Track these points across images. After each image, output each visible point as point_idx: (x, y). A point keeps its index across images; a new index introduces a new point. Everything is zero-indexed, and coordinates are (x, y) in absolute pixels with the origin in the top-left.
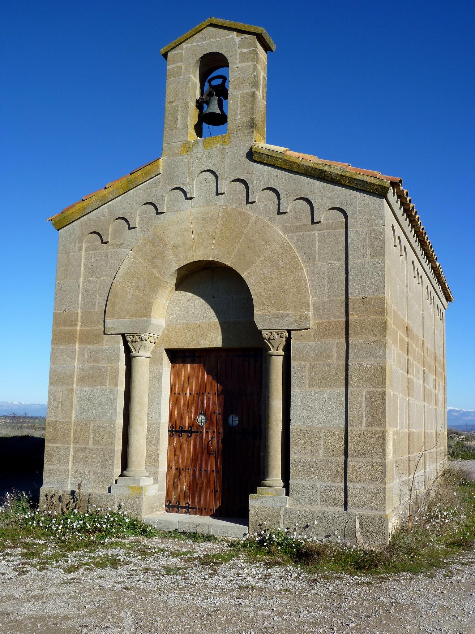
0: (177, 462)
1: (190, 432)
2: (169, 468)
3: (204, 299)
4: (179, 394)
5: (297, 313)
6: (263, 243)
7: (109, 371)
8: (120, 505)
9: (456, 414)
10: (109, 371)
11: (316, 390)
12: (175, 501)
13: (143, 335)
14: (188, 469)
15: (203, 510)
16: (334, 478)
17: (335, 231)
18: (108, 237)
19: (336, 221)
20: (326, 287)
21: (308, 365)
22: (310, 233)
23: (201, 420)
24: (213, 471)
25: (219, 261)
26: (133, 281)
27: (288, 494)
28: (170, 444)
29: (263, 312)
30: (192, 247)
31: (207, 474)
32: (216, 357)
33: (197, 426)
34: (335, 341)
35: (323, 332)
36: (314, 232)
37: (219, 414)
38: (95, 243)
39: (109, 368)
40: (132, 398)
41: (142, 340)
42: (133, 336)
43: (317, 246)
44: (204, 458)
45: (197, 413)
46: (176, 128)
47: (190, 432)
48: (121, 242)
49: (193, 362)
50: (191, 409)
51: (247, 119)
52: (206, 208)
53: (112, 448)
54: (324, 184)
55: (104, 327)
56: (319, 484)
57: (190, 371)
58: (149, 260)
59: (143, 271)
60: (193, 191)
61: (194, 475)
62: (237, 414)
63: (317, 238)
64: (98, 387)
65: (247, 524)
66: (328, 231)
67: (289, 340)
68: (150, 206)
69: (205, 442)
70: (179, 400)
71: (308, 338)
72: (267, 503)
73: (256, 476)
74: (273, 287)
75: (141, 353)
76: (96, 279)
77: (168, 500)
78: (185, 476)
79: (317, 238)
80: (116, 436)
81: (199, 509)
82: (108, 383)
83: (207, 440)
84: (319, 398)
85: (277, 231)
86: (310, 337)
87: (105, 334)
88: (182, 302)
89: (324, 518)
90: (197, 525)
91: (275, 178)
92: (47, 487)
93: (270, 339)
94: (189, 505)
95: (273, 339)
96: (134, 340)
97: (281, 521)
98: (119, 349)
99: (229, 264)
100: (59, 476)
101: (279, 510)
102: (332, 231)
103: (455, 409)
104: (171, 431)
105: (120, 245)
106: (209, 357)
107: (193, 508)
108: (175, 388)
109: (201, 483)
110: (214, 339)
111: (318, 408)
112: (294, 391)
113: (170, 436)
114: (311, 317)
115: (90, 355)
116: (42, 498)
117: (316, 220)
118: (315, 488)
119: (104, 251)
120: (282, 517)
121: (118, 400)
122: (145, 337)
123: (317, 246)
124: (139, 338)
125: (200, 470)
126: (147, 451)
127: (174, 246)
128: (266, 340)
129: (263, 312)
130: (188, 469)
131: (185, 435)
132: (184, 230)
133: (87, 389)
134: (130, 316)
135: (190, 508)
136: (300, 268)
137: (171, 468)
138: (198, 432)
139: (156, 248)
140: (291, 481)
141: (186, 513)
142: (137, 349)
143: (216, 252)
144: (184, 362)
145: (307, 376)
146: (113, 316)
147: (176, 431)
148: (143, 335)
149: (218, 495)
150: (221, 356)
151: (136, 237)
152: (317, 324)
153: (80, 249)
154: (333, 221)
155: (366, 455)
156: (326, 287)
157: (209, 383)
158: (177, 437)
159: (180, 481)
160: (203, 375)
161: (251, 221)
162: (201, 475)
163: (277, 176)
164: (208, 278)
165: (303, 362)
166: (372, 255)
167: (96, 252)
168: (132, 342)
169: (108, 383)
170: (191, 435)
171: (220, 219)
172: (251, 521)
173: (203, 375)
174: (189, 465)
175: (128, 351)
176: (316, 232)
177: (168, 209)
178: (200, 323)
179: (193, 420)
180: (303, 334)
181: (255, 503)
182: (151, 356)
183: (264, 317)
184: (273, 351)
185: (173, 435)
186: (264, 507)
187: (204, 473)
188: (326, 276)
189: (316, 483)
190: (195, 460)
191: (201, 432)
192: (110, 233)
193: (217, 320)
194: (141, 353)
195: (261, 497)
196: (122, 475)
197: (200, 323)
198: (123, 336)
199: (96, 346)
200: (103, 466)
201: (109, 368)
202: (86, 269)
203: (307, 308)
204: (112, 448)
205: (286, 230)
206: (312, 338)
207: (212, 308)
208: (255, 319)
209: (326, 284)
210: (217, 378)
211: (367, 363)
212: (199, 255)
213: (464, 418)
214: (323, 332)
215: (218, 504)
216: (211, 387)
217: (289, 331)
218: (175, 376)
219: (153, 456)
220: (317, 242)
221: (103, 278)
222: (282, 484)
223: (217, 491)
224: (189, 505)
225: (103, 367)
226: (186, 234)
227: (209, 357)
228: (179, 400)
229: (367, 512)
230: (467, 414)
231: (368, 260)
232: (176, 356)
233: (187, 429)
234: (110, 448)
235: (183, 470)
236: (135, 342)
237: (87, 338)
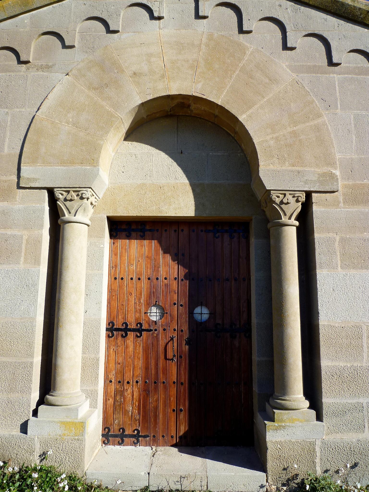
0: (121, 372)
1: (139, 330)
2: (108, 381)
3: (167, 153)
4: (122, 279)
5: (319, 170)
6: (267, 81)
7: (24, 242)
8: (44, 454)
10: (24, 242)
11: (353, 272)
12: (117, 428)
13: (84, 191)
14: (137, 382)
15: (161, 438)
17: (359, 77)
18: (29, 54)
19: (359, 65)
20: (354, 142)
21: (338, 238)
22: (327, 76)
23: (154, 314)
24: (174, 383)
25: (204, 97)
26: (70, 115)
27: (319, 418)
28: (108, 348)
29: (272, 167)
30: (163, 76)
31: (165, 387)
32: (175, 231)
33: (150, 322)
36: (332, 75)
37: (181, 305)
38: (6, 63)
39: (25, 237)
40: (63, 283)
41: (82, 198)
42: (68, 192)
43: (338, 92)
44: (161, 365)
45: (149, 305)
47: (139, 330)
48: (50, 64)
49: (143, 237)
50: (140, 299)
52: (183, 31)
53: (29, 360)
54: (342, 22)
55: (19, 177)
57: (139, 250)
58: (95, 89)
59: (87, 103)
61: (146, 392)
62: (206, 306)
63: (337, 83)
64: (5, 266)
66: (350, 76)
68: (97, 22)
70: (121, 287)
71: (336, 204)
74: (284, 136)
75: (79, 217)
76: (6, 110)
78: (132, 392)
79: (337, 83)
80: (36, 341)
81: (154, 436)
82: (22, 259)
83: (166, 341)
84: (356, 282)
86: (339, 202)
87: (19, 187)
88: (134, 157)
90: (181, 477)
91: (278, 8)
93: (282, 202)
94: (138, 432)
95: (288, 203)
96: (69, 197)
97: (318, 460)
98: (43, 210)
99: (219, 102)
101: (313, 444)
102: (355, 76)
104: (111, 329)
105: (48, 68)
106: (166, 230)
107: (145, 437)
108: (115, 270)
109: (157, 400)
110: (181, 203)
111: (356, 296)
112: (323, 277)
113: (108, 337)
114: (339, 177)
117: (335, 60)
119: (22, 73)
120: (318, 454)
121: (40, 286)
122: (88, 193)
123: (338, 92)
124: (78, 195)
125: (155, 383)
126: (83, 359)
127: (135, 74)
128: (276, 204)
129: (272, 167)
130: (137, 382)
131: (131, 335)
132: (150, 55)
134: (63, 163)
135: (141, 436)
137: (111, 381)
138: (151, 330)
141: (135, 444)
142: (73, 212)
143: (200, 86)
144: (129, 237)
145: (338, 254)
146: (34, 161)
147: (118, 330)
148: (84, 191)
149: (182, 416)
150: (182, 230)
151: (76, 57)
152: (346, 186)
154: (355, 65)
156: (354, 142)
157: (166, 264)
158: (120, 338)
159: (125, 399)
160: (157, 254)
161: (248, 53)
162: (156, 389)
163: (280, 6)
164: (180, 123)
165: (331, 235)
167: (8, 74)
168: (66, 200)
169: (22, 259)
170: (141, 335)
171: (203, 47)
172: (270, 464)
173: (157, 254)
174: (137, 376)
175: (55, 213)
176: (335, 76)
177: (123, 29)
178: (166, 188)
179: (143, 314)
180: (328, 199)
182: (89, 222)
183: (275, 173)
184: (284, 219)
185: (113, 335)
186: (290, 441)
187: (161, 386)
188: (353, 128)
189: (361, 400)
190: (147, 368)
191: (156, 330)
192: (32, 50)
193: (187, 181)
194: (79, 217)
195: (284, 427)
196: (41, 401)
197: (166, 188)
198: (51, 192)
200: (11, 390)
201: (25, 237)
204: (29, 360)
205: (296, 70)
206: (342, 205)
207: (179, 165)
209: (354, 137)
210: (177, 258)
212: (175, 88)
215: (183, 429)
216: (169, 269)
217: (309, 194)
218: (116, 255)
219: (88, 366)
220: (337, 87)
221: (18, 110)
222: (307, 404)
223: (181, 410)
224: (138, 432)
225: (14, 236)
226: (153, 59)
227: (166, 230)
228: (121, 287)
232: (120, 228)
233: (133, 326)
234: (24, 360)
235: (128, 383)
236: (71, 200)
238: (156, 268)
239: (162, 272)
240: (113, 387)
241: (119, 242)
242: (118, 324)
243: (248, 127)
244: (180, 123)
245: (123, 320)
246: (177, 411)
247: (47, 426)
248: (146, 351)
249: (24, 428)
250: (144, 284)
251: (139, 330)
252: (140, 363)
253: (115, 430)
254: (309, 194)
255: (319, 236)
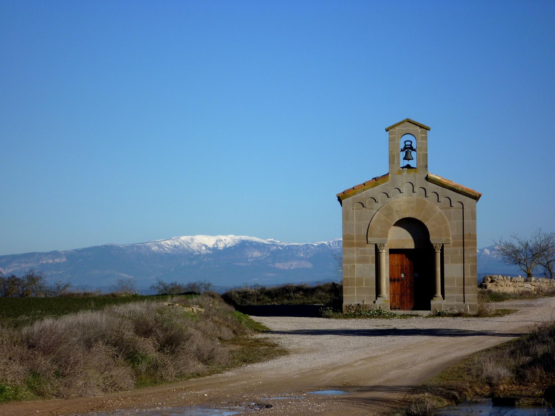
0: (394, 292)
9: (256, 254)
16: (460, 293)
27: (444, 299)
34: (459, 248)
35: (455, 245)
45: (401, 273)
46: (394, 163)
51: (424, 164)
56: (455, 295)
57: (397, 257)
60: (403, 190)
61: (401, 297)
65: (430, 309)
67: (443, 247)
69: (405, 284)
71: (450, 247)
72: (437, 302)
73: (433, 294)
77: (391, 307)
78: (397, 297)
85: (438, 209)
89: (458, 306)
92: (345, 303)
100: (350, 299)
103: (255, 239)
110: (411, 245)
112: (445, 265)
115: (361, 251)
116: (344, 308)
118: (454, 297)
131: (396, 282)
133: (360, 265)
134: (378, 237)
136: (446, 222)
139: (389, 211)
140: (445, 295)
146: (371, 237)
151: (379, 205)
153: (353, 209)
155: (470, 285)
164: (411, 224)
166: (472, 219)
176: (452, 210)
178: (404, 239)
181: (433, 303)
183: (433, 239)
190: (401, 291)
197: (404, 239)
198: (376, 245)
199: (363, 248)
202: (356, 217)
203: (449, 236)
205: (441, 208)
208: (431, 240)
211: (470, 256)
212: (407, 216)
213: (277, 265)
214: (455, 245)
216: (406, 262)
217: (443, 244)
229: (472, 303)
230: (288, 253)
231: (471, 221)
232: (392, 252)
237: (359, 245)
238: (403, 262)
239: (405, 263)
240: (392, 296)
241: (392, 255)
242: (393, 279)
243: (427, 226)
244: (411, 224)
245: (250, 256)
246: (410, 302)
247: (379, 301)
248: (401, 285)
249: (374, 302)
250: (400, 267)
251: (398, 280)
252: (399, 289)
253: (393, 307)
254: (443, 244)
255: (389, 338)
